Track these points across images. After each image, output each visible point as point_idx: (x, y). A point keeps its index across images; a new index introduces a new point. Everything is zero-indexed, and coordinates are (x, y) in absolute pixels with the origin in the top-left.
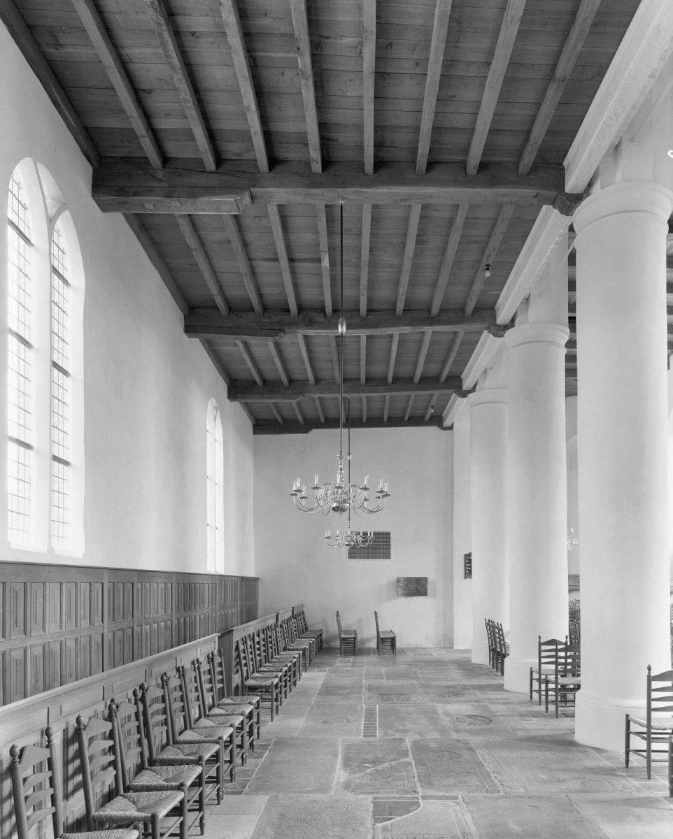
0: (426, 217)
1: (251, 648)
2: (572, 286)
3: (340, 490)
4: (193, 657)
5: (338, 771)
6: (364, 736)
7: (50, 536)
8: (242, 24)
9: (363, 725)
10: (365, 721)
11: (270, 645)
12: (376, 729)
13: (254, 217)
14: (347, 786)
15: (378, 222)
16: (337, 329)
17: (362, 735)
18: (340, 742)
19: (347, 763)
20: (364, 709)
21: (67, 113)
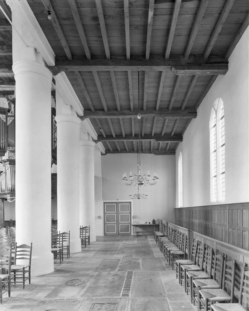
0: (99, 37)
1: (171, 234)
2: (54, 112)
3: (140, 177)
4: (200, 240)
5: (141, 262)
6: (132, 272)
7: (217, 197)
8: (171, 24)
9: (133, 278)
10: (131, 281)
11: (181, 242)
12: (127, 275)
13: (181, 35)
14: (138, 259)
15: (122, 33)
16: (141, 118)
17: (133, 273)
18: (142, 270)
19: (139, 263)
20: (131, 291)
21: (214, 79)
